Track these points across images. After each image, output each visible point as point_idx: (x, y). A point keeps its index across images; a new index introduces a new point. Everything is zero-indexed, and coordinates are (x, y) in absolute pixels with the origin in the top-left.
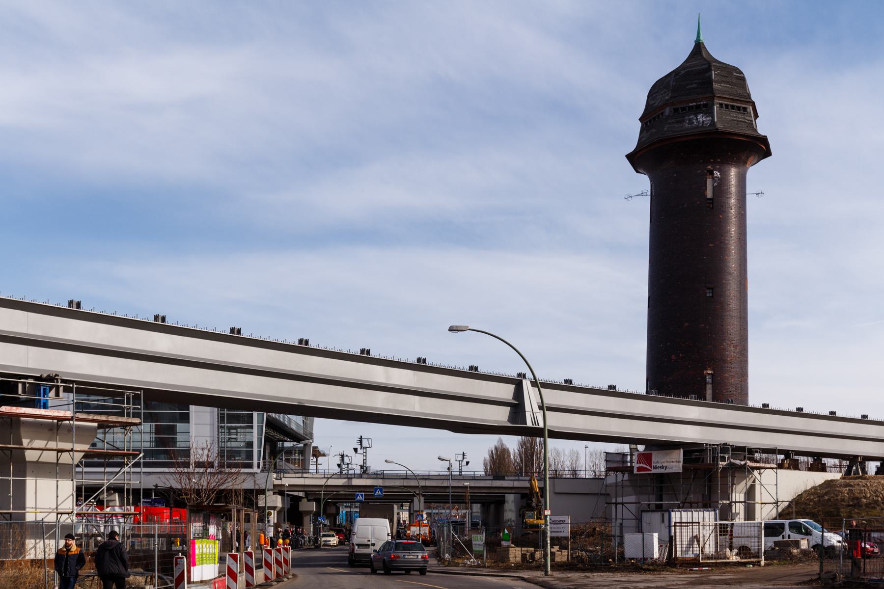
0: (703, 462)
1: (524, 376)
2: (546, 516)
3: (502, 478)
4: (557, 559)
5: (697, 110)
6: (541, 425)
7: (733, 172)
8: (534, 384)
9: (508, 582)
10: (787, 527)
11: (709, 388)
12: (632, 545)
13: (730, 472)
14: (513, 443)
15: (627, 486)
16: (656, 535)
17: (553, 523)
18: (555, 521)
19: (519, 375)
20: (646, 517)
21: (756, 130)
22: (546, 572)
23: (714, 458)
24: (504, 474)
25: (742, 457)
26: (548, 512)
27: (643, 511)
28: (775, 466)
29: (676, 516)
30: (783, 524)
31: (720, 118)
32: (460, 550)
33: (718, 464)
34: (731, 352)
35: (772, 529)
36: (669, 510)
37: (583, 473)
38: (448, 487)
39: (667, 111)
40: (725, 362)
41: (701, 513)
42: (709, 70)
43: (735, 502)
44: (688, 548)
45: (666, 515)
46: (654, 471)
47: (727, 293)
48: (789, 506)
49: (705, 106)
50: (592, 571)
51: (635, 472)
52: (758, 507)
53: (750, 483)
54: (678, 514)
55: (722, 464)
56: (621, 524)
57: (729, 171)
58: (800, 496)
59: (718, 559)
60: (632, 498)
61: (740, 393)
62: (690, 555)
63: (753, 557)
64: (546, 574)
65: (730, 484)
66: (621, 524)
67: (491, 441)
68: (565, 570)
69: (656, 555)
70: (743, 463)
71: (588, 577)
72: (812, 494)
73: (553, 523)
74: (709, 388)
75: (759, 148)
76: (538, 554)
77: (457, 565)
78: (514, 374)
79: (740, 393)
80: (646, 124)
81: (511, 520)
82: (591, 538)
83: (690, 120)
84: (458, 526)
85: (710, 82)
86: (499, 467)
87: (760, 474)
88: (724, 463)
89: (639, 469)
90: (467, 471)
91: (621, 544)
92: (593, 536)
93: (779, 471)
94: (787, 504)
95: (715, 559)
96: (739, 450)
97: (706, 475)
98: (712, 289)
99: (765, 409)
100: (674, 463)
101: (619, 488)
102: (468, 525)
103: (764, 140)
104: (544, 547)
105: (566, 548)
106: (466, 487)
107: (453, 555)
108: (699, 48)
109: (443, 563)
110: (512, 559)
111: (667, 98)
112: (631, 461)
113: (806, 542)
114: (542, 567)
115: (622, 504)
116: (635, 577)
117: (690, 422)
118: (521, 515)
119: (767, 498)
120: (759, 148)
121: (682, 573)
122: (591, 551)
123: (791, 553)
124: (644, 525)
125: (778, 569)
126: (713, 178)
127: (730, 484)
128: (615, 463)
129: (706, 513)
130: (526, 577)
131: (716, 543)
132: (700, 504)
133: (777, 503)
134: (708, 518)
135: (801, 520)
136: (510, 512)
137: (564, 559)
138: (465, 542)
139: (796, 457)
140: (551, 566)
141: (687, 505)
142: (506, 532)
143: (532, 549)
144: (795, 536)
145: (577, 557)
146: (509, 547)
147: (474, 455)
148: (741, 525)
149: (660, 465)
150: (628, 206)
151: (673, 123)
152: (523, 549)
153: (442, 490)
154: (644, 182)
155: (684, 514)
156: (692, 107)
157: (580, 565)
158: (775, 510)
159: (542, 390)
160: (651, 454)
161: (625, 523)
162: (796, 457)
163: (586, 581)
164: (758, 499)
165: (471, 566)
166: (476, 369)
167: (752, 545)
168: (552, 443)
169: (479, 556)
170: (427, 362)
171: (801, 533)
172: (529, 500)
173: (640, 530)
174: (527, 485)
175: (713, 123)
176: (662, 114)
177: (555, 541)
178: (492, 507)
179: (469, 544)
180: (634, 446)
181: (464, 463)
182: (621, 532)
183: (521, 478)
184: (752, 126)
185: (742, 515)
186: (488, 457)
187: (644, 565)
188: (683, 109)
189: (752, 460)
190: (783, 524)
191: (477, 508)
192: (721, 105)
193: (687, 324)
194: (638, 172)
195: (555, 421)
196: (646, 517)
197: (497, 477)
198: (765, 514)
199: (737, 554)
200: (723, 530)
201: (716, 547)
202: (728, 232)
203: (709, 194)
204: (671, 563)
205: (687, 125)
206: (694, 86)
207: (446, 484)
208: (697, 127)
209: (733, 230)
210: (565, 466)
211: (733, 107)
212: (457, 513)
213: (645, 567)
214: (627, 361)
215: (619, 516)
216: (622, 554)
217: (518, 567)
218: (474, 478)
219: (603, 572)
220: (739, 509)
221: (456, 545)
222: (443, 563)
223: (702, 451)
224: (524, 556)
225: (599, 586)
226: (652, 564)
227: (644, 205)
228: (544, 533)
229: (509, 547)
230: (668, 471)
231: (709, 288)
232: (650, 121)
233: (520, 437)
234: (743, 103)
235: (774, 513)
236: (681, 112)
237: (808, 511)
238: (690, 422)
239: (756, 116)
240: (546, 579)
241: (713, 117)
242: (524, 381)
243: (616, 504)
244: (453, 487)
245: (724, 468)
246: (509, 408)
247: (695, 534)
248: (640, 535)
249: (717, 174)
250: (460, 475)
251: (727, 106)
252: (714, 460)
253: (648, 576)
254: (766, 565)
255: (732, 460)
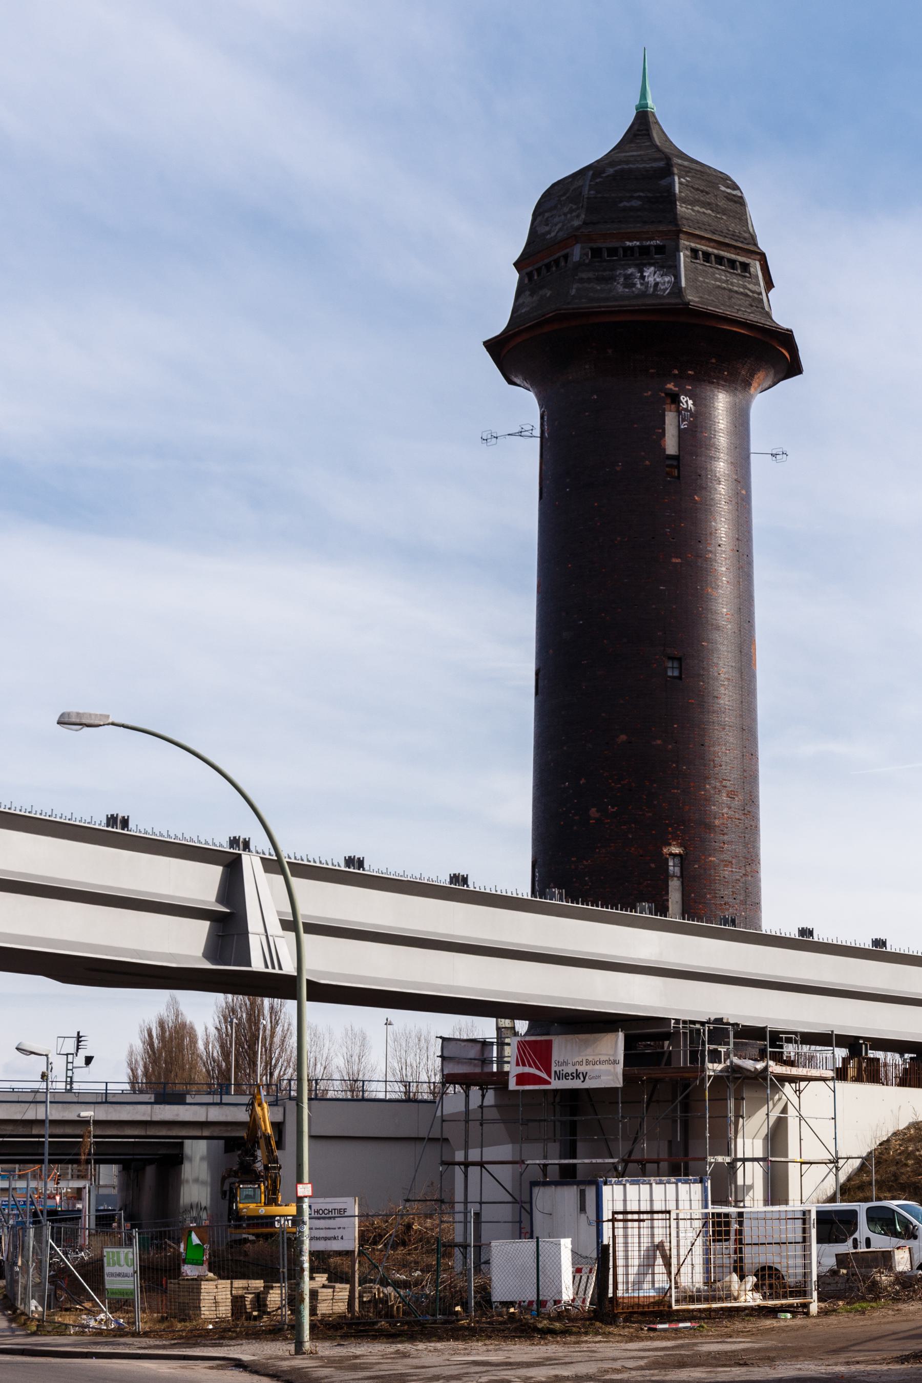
0: (669, 1062)
1: (246, 845)
2: (300, 1200)
3: (178, 1099)
4: (323, 1308)
5: (643, 257)
6: (289, 968)
7: (722, 403)
8: (273, 865)
9: (199, 1370)
10: (862, 1219)
11: (674, 886)
12: (508, 1270)
13: (732, 1087)
14: (204, 1014)
15: (494, 1121)
16: (566, 1244)
17: (318, 1215)
18: (318, 1210)
19: (234, 842)
20: (543, 1197)
21: (768, 315)
22: (299, 1344)
23: (694, 1054)
24: (180, 1088)
25: (755, 1052)
26: (304, 1190)
27: (534, 1184)
28: (830, 1074)
29: (614, 1196)
30: (854, 1213)
31: (693, 280)
32: (74, 1285)
33: (703, 1070)
34: (723, 807)
35: (833, 1226)
36: (594, 1181)
37: (373, 1086)
38: (41, 1122)
39: (577, 253)
40: (709, 827)
41: (671, 1188)
42: (667, 171)
43: (744, 1160)
44: (641, 1274)
45: (591, 1192)
46: (556, 1084)
47: (713, 671)
48: (862, 1168)
49: (660, 249)
50: (412, 1338)
51: (512, 1085)
52: (793, 1170)
53: (775, 1114)
54: (619, 1189)
55: (713, 1068)
56: (478, 1215)
57: (713, 398)
58: (885, 1144)
59: (714, 1299)
60: (504, 1151)
61: (744, 902)
62: (647, 1292)
63: (793, 1294)
64: (299, 1350)
65: (731, 1115)
66: (478, 1215)
67: (149, 1007)
68: (345, 1337)
69: (567, 1295)
70: (760, 1066)
71: (405, 1355)
72: (911, 1139)
73: (318, 1215)
74: (674, 886)
75: (777, 354)
76: (275, 1297)
77: (61, 1330)
78: (221, 842)
79: (744, 902)
80: (530, 275)
81: (199, 1207)
82: (401, 1251)
83: (628, 277)
84: (63, 1221)
85: (669, 199)
86: (168, 1071)
87: (798, 1092)
88: (719, 1067)
89: (522, 1079)
90: (88, 1080)
91: (482, 1264)
92: (404, 1244)
93: (840, 1085)
94: (857, 1163)
95: (707, 1300)
96: (767, 1041)
97: (675, 1094)
98: (679, 660)
99: (805, 941)
100: (602, 1065)
101: (474, 1126)
102: (88, 1221)
103: (787, 339)
104: (295, 1274)
105: (345, 1278)
106: (85, 1123)
107: (53, 1303)
108: (643, 124)
109: (24, 1325)
110: (207, 1311)
111: (576, 223)
112: (501, 1061)
113: (907, 1255)
114: (284, 1330)
115: (481, 1164)
116: (521, 1351)
117: (634, 967)
118: (226, 1193)
119: (814, 1151)
120: (777, 354)
121: (631, 1339)
122: (405, 1285)
123: (875, 1284)
124: (538, 1217)
125: (847, 1322)
126: (679, 411)
127: (731, 1115)
128: (466, 1067)
129: (683, 1188)
130: (245, 1358)
131: (707, 1262)
132: (664, 1165)
133: (835, 1161)
134: (687, 1198)
135: (893, 1204)
136: (196, 1184)
137: (342, 1307)
138: (81, 1266)
139: (872, 1054)
140: (313, 1327)
141: (637, 1168)
142: (195, 1240)
143: (259, 1284)
144: (881, 1242)
145: (374, 1301)
146: (199, 1279)
147: (110, 1037)
148: (757, 1217)
149: (570, 1069)
150: (490, 461)
151: (589, 280)
152: (238, 1283)
153: (21, 1130)
154: (524, 406)
155: (632, 1190)
156: (631, 248)
157: (383, 1323)
158: (832, 1177)
159: (295, 881)
160: (549, 1044)
161: (488, 1213)
162: (872, 1054)
163: (401, 1367)
164: (793, 1153)
165: (99, 1333)
166: (125, 823)
167: (789, 1264)
168: (318, 1013)
169: (120, 1304)
170: (131, 825)
171: (896, 1235)
172: (246, 1155)
173: (524, 1228)
174: (242, 1115)
175: (677, 289)
176: (566, 257)
177: (321, 1261)
178: (150, 1172)
179: (94, 1271)
180: (506, 1023)
181: (80, 1060)
182: (478, 1236)
183: (226, 1099)
184: (758, 304)
185: (758, 1192)
186: (139, 1046)
187: (533, 1321)
188: (613, 251)
189: (778, 1058)
190: (854, 1213)
191: (109, 1174)
192: (694, 252)
193: (623, 737)
194: (511, 382)
195: (327, 961)
196: (543, 1197)
197: (163, 1098)
198: (810, 1189)
199: (756, 1288)
200: (719, 1229)
201: (707, 1271)
202: (712, 534)
203: (671, 446)
204: (606, 1312)
205: (620, 289)
206: (636, 203)
207: (38, 1113)
208: (643, 294)
209: (722, 529)
210: (332, 1068)
211: (720, 260)
212: (56, 1187)
213: (544, 1324)
214: (491, 817)
215: (473, 1196)
216: (484, 1291)
217: (223, 1333)
218: (105, 1099)
219: (440, 1339)
220: (752, 1176)
221: (60, 1274)
222: (24, 1325)
223: (667, 1036)
224: (237, 1302)
225: (437, 1378)
226: (560, 1316)
227: (525, 462)
228: (294, 1242)
229: (199, 1279)
230: (590, 1084)
231: (672, 658)
232: (539, 270)
233: (220, 996)
234: (740, 253)
235: (830, 1187)
236: (608, 257)
237: (903, 1179)
238: (634, 967)
239: (769, 285)
240: (299, 1362)
241: (677, 277)
242: (246, 858)
243: (467, 1164)
244: (53, 1122)
245: (717, 1079)
246: (207, 924)
247: (657, 1240)
248: (530, 1245)
249: (687, 402)
250: (69, 1091)
251: (707, 256)
252: (694, 1059)
253: (550, 1349)
254: (823, 1313)
255: (736, 1060)
